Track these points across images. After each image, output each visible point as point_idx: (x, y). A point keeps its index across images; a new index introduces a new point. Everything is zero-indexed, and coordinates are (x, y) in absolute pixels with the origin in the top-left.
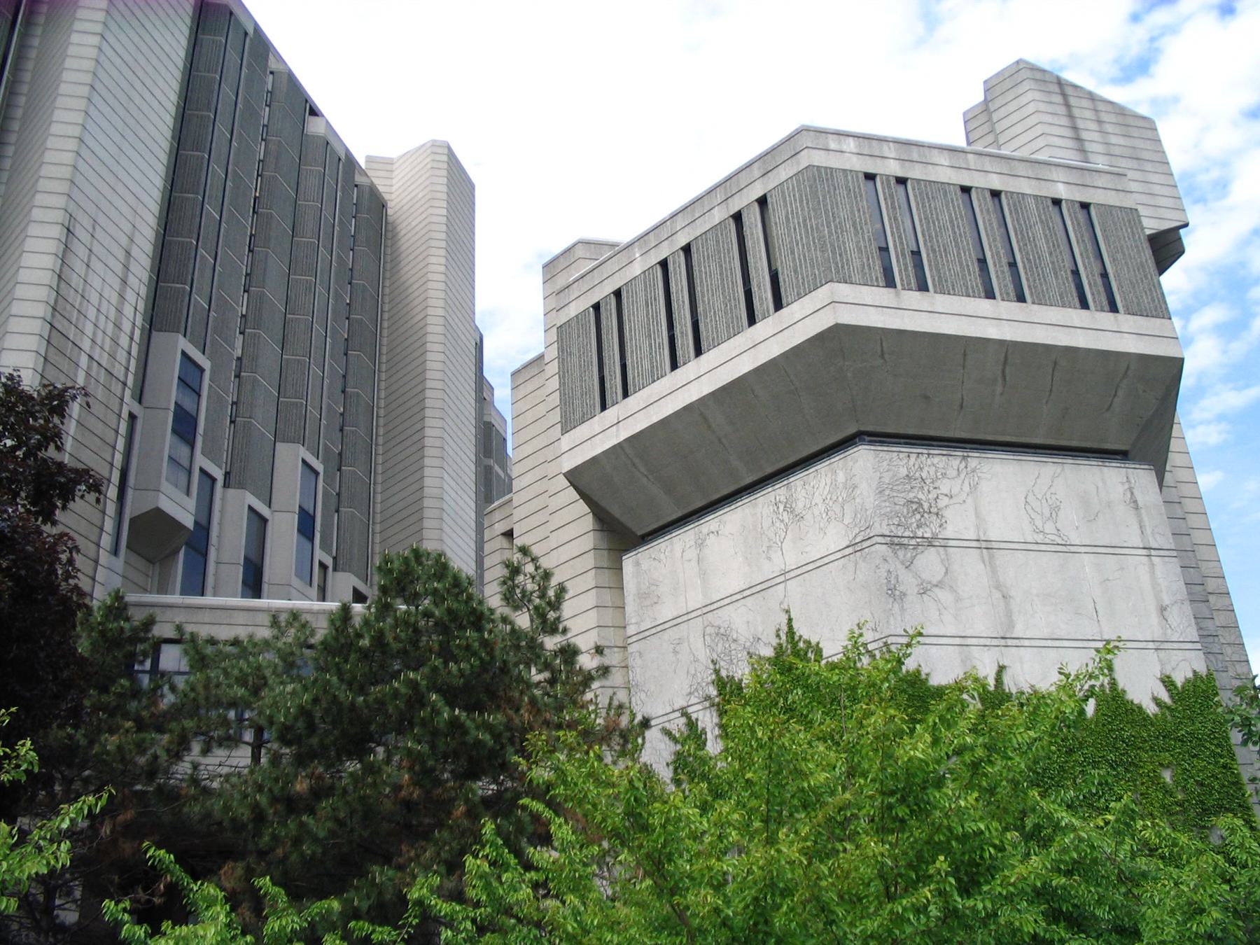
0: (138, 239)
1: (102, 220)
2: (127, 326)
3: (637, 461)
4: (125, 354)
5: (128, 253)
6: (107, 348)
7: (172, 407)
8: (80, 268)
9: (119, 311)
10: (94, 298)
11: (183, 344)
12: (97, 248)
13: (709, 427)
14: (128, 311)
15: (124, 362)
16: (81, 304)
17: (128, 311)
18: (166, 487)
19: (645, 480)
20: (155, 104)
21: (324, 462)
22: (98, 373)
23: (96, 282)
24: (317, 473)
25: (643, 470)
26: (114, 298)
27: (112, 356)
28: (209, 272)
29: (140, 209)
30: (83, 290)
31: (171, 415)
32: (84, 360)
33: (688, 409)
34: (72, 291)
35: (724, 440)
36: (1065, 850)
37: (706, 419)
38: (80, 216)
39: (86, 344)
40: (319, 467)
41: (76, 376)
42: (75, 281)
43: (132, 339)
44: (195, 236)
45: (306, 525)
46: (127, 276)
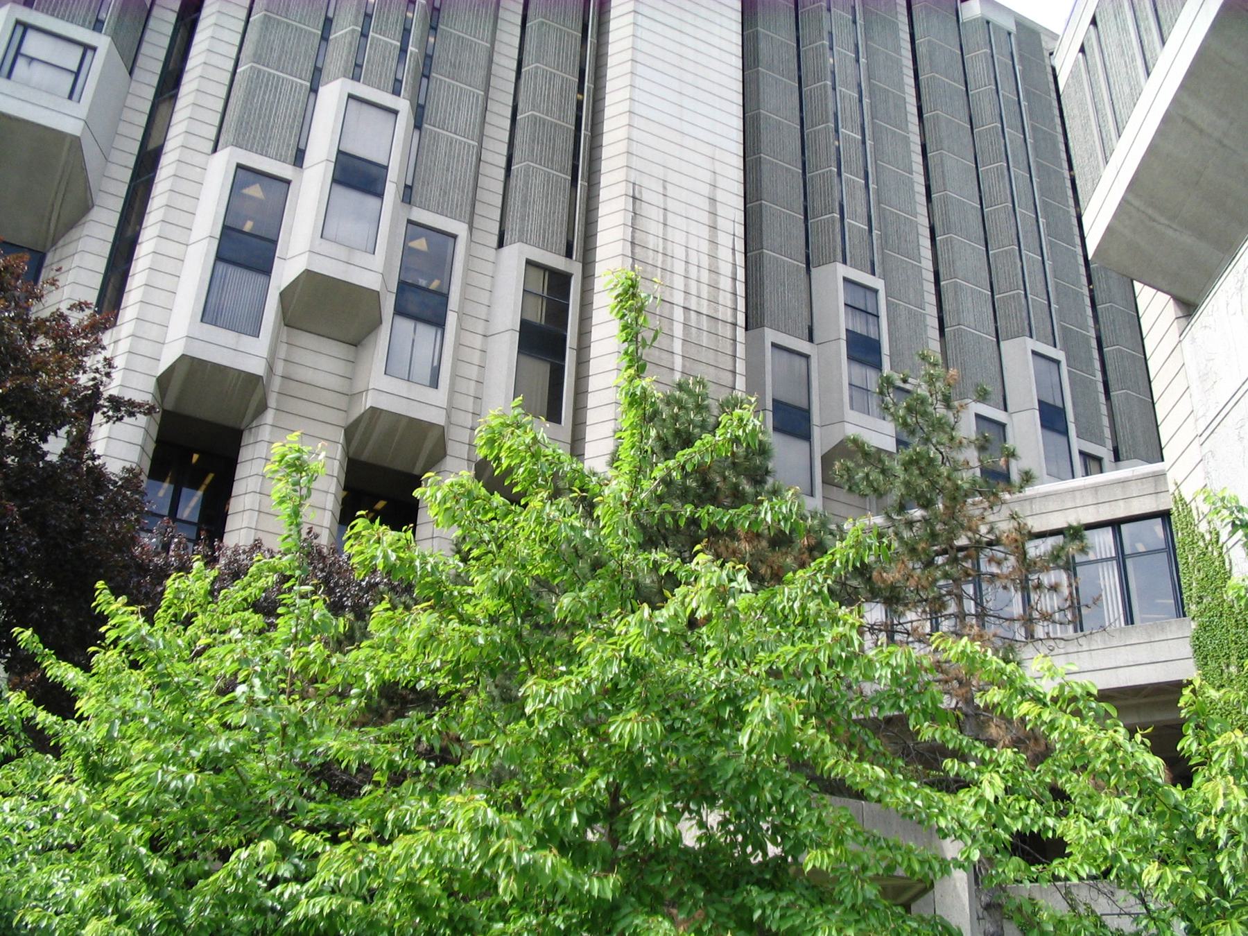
0: (721, 182)
1: (672, 177)
2: (726, 269)
3: (1150, 211)
4: (729, 296)
5: (713, 200)
6: (705, 294)
7: (843, 335)
8: (655, 228)
9: (713, 257)
10: (679, 252)
11: (842, 270)
12: (671, 205)
13: (1201, 131)
14: (725, 254)
15: (729, 304)
16: (663, 262)
17: (725, 254)
18: (851, 415)
19: (1170, 233)
20: (715, 53)
21: (1066, 349)
22: (698, 322)
23: (677, 236)
24: (1058, 362)
25: (1163, 220)
26: (705, 246)
27: (714, 301)
28: (861, 194)
29: (718, 154)
30: (664, 248)
31: (843, 345)
32: (678, 314)
33: (1167, 119)
34: (651, 253)
35: (1226, 141)
36: (1052, 726)
37: (1193, 124)
38: (645, 181)
39: (678, 298)
40: (1059, 354)
41: (672, 330)
42: (651, 242)
43: (734, 279)
44: (834, 163)
45: (1052, 418)
46: (715, 222)
